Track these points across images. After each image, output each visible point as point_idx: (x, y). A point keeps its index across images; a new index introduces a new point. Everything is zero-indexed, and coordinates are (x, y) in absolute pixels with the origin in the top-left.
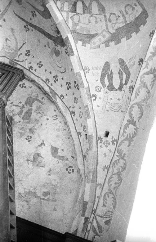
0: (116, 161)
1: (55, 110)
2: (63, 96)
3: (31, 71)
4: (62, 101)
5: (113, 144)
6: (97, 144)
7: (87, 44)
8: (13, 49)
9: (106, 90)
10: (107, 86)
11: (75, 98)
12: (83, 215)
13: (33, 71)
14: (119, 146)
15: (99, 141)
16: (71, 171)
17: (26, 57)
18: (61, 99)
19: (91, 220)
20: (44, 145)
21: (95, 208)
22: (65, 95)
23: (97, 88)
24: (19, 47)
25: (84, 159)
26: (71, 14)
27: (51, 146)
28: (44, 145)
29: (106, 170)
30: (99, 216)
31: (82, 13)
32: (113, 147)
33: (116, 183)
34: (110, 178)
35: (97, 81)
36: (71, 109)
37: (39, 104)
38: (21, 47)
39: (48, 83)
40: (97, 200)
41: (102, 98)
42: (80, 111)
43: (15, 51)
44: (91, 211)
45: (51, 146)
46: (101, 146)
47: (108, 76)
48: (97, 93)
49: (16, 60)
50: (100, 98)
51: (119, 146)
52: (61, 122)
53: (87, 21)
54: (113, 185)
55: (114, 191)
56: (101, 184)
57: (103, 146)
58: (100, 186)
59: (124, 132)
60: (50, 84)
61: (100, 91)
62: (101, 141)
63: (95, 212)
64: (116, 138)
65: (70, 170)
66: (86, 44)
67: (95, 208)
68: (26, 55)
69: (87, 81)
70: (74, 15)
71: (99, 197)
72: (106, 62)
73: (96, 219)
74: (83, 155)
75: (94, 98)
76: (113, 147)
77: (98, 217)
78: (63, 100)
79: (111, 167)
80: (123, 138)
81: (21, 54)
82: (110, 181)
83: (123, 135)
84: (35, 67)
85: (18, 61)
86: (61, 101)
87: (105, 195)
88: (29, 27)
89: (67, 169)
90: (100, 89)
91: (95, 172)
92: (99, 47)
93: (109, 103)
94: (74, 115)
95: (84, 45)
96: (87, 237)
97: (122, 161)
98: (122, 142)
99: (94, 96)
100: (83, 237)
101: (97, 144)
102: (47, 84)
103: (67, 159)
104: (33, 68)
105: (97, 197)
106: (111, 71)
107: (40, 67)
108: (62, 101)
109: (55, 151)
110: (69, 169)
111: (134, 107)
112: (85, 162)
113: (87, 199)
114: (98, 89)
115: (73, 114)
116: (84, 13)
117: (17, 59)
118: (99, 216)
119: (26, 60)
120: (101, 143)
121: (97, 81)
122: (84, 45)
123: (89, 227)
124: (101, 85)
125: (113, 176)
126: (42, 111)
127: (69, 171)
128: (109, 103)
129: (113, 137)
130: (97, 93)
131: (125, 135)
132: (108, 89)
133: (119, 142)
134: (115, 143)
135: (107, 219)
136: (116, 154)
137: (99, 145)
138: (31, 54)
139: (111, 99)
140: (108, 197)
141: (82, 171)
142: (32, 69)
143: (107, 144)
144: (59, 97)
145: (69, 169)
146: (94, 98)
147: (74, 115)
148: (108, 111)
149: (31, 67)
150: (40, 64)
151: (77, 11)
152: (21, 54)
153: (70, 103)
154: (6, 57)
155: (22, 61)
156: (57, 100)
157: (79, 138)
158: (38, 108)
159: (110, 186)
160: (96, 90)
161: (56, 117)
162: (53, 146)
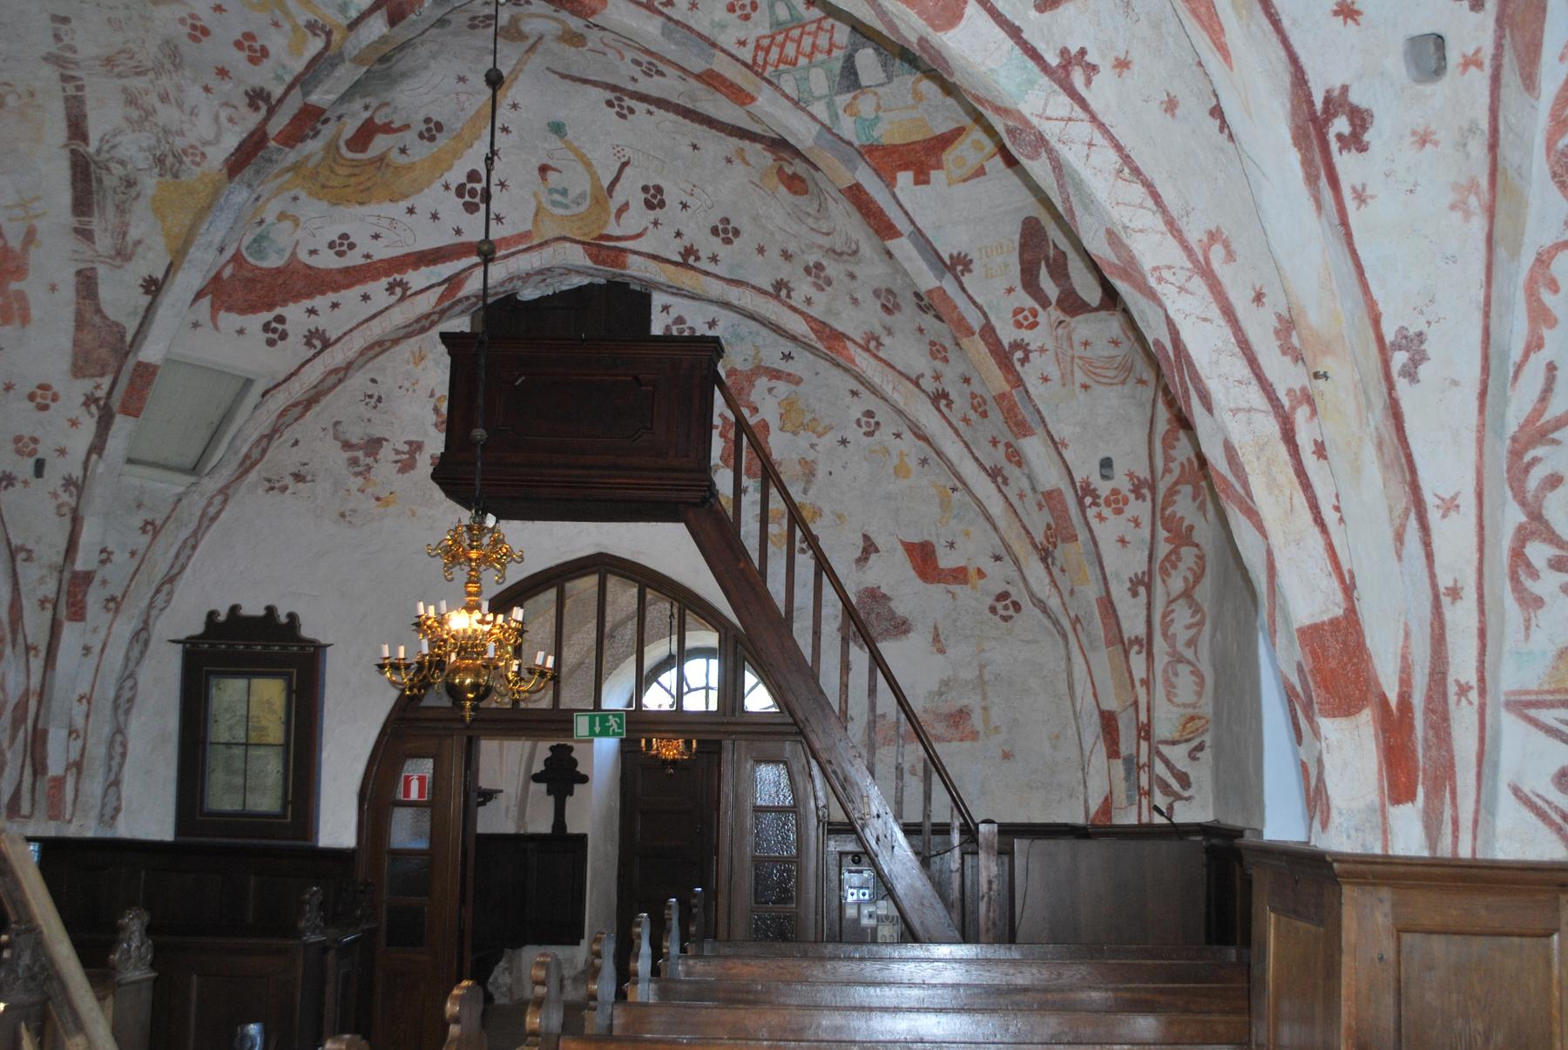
0: (1167, 557)
1: (854, 393)
2: (877, 339)
3: (697, 265)
4: (881, 360)
5: (1139, 496)
6: (1084, 512)
7: (934, 174)
8: (583, 196)
9: (1056, 314)
10: (1054, 301)
11: (933, 344)
12: (1113, 753)
13: (701, 265)
14: (1163, 509)
15: (1088, 500)
16: (1011, 612)
17: (652, 215)
18: (867, 350)
19: (1144, 759)
20: (877, 551)
21: (1143, 718)
22: (878, 330)
23: (1020, 317)
24: (606, 183)
25: (1044, 560)
26: (843, 100)
27: (903, 543)
28: (877, 551)
29: (1142, 590)
30: (1166, 742)
31: (882, 76)
32: (1142, 509)
33: (1189, 627)
34: (1164, 616)
35: (1010, 290)
36: (928, 384)
37: (782, 387)
38: (617, 179)
39: (789, 296)
40: (1141, 692)
41: (1050, 345)
42: (966, 389)
43: (597, 200)
44: (1134, 732)
45: (903, 543)
46: (1100, 516)
47: (1048, 266)
48: (1026, 335)
49: (609, 238)
50: (1042, 350)
51: (1163, 509)
52: (898, 435)
53: (910, 100)
54: (1183, 636)
55: (1189, 654)
56: (1137, 641)
57: (1106, 512)
58: (1136, 648)
59: (1168, 459)
60: (797, 300)
61: (1033, 325)
62: (1096, 497)
63: (1148, 733)
64: (1143, 473)
65: (1006, 608)
66: (928, 175)
67: (1143, 718)
68: (649, 205)
69: (974, 303)
70: (855, 98)
71: (1146, 682)
72: (1024, 223)
73: (1159, 754)
74: (1035, 546)
75: (1019, 354)
76: (1142, 509)
77: (1164, 749)
78: (881, 354)
79: (1158, 579)
80: (1170, 479)
81: (624, 208)
82: (1166, 626)
83: (1167, 470)
84: (708, 245)
85: (618, 239)
86: (873, 361)
87: (1165, 671)
88: (628, 102)
89: (993, 610)
90: (1031, 319)
91: (1108, 606)
92: (981, 172)
93: (1081, 358)
94: (948, 406)
95: (922, 178)
96: (533, 750)
97: (1186, 551)
98: (1172, 491)
99: (1016, 345)
100: (238, 808)
101: (1084, 512)
102: (784, 304)
103: (981, 574)
104: (701, 254)
105: (1137, 684)
106: (1055, 246)
107: (728, 241)
108: (881, 360)
109: (924, 560)
110: (999, 606)
111: (1178, 492)
112: (1056, 571)
113: (1110, 704)
114: (1026, 318)
115: (943, 402)
116: (890, 78)
117: (617, 232)
118: (1166, 742)
119: (656, 223)
120: (1094, 504)
121: (1010, 290)
122: (922, 178)
123: (1144, 782)
124: (1029, 302)
125: (1173, 606)
126: (809, 416)
127: (1002, 612)
128: (1081, 358)
129: (1131, 475)
130: (1026, 335)
131: (1175, 466)
132: (1063, 310)
133: (1162, 489)
134: (1145, 491)
135: (1195, 743)
136: (1162, 534)
137: (1091, 512)
138: (672, 196)
139: (1086, 344)
140: (1176, 675)
141: (1054, 602)
142: (697, 259)
143: (1116, 502)
144: (860, 346)
145: (999, 606)
146: (1019, 354)
147: (948, 406)
148: (1085, 387)
149: (689, 252)
150: (725, 231)
151: (865, 80)
152: (624, 208)
153: (915, 358)
154: (565, 239)
155: (639, 236)
156: (857, 360)
157: (1000, 491)
158: (789, 408)
159: (1173, 646)
160: (1019, 325)
161: (872, 421)
162: (908, 540)
